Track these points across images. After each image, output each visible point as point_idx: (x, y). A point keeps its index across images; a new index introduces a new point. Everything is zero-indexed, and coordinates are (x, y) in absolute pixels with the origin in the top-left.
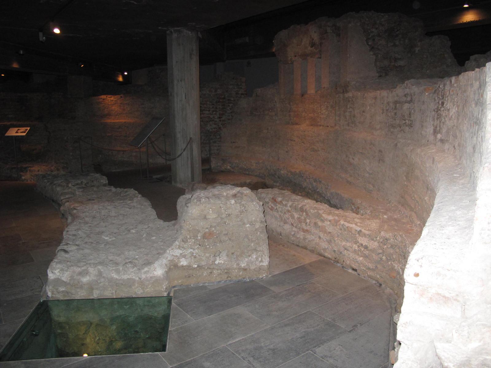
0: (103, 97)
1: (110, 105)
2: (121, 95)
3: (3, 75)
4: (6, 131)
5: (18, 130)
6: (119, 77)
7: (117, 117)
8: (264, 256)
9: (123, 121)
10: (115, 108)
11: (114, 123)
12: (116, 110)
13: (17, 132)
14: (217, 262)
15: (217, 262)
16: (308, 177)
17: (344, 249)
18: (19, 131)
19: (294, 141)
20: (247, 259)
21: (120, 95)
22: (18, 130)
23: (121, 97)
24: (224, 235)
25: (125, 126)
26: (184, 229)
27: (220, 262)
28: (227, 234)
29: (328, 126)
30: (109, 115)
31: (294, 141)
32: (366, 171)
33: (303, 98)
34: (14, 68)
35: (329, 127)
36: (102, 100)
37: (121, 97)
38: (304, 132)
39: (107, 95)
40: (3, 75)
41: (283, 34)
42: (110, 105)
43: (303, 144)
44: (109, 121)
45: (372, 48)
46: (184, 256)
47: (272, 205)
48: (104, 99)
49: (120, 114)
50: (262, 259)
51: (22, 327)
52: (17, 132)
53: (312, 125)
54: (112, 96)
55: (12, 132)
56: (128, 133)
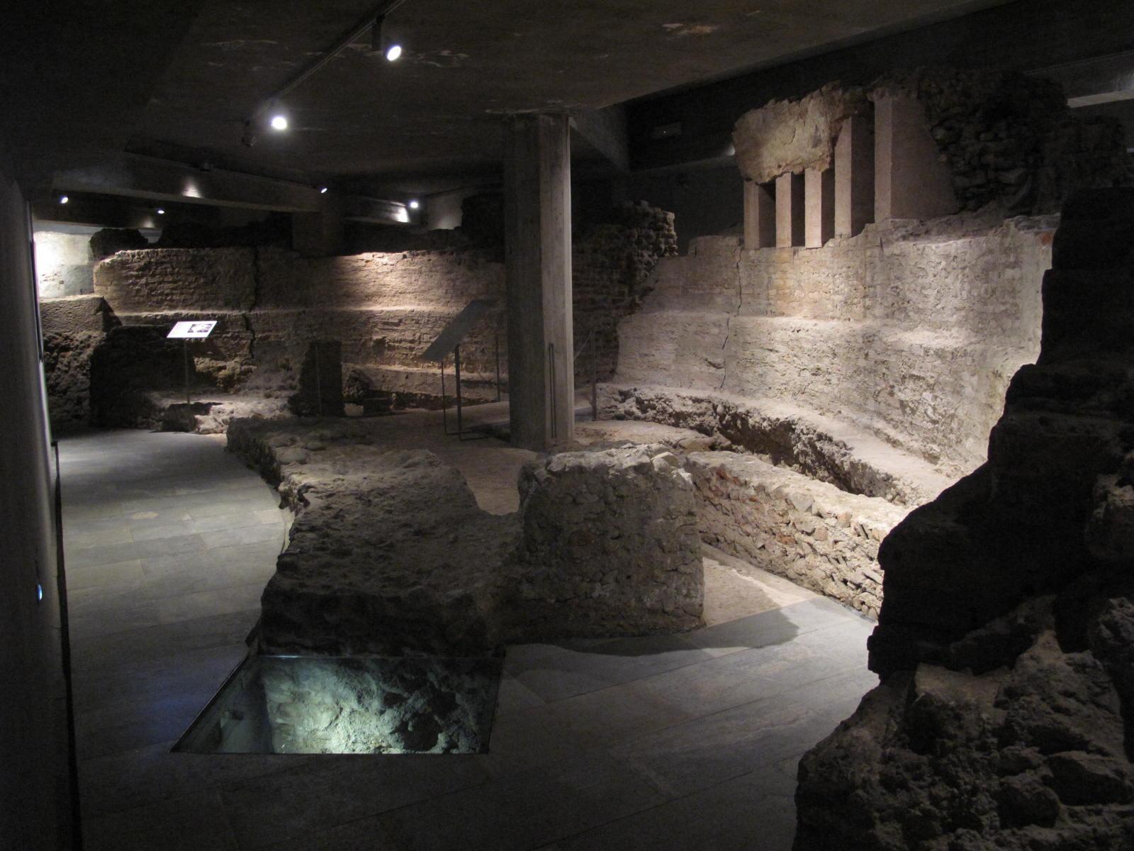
0: (366, 256)
1: (380, 274)
2: (405, 253)
3: (324, 191)
4: (168, 330)
5: (194, 325)
6: (397, 212)
7: (395, 299)
8: (693, 584)
9: (408, 308)
10: (393, 281)
11: (388, 312)
12: (394, 284)
13: (190, 331)
14: (596, 594)
15: (596, 594)
16: (805, 432)
17: (864, 577)
18: (193, 329)
19: (777, 351)
20: (657, 591)
21: (401, 252)
22: (194, 325)
23: (405, 257)
24: (612, 538)
25: (413, 320)
26: (287, 463)
27: (602, 593)
28: (618, 537)
29: (849, 320)
30: (369, 297)
31: (777, 351)
32: (928, 416)
33: (796, 257)
34: (191, 198)
35: (852, 320)
36: (363, 263)
37: (405, 257)
38: (798, 331)
39: (374, 253)
40: (324, 191)
41: (753, 118)
42: (380, 274)
43: (795, 358)
44: (376, 308)
45: (944, 146)
46: (531, 581)
47: (718, 485)
48: (367, 261)
49: (401, 293)
50: (689, 590)
51: (37, 568)
52: (190, 331)
53: (815, 317)
54: (385, 254)
55: (181, 331)
56: (418, 334)
